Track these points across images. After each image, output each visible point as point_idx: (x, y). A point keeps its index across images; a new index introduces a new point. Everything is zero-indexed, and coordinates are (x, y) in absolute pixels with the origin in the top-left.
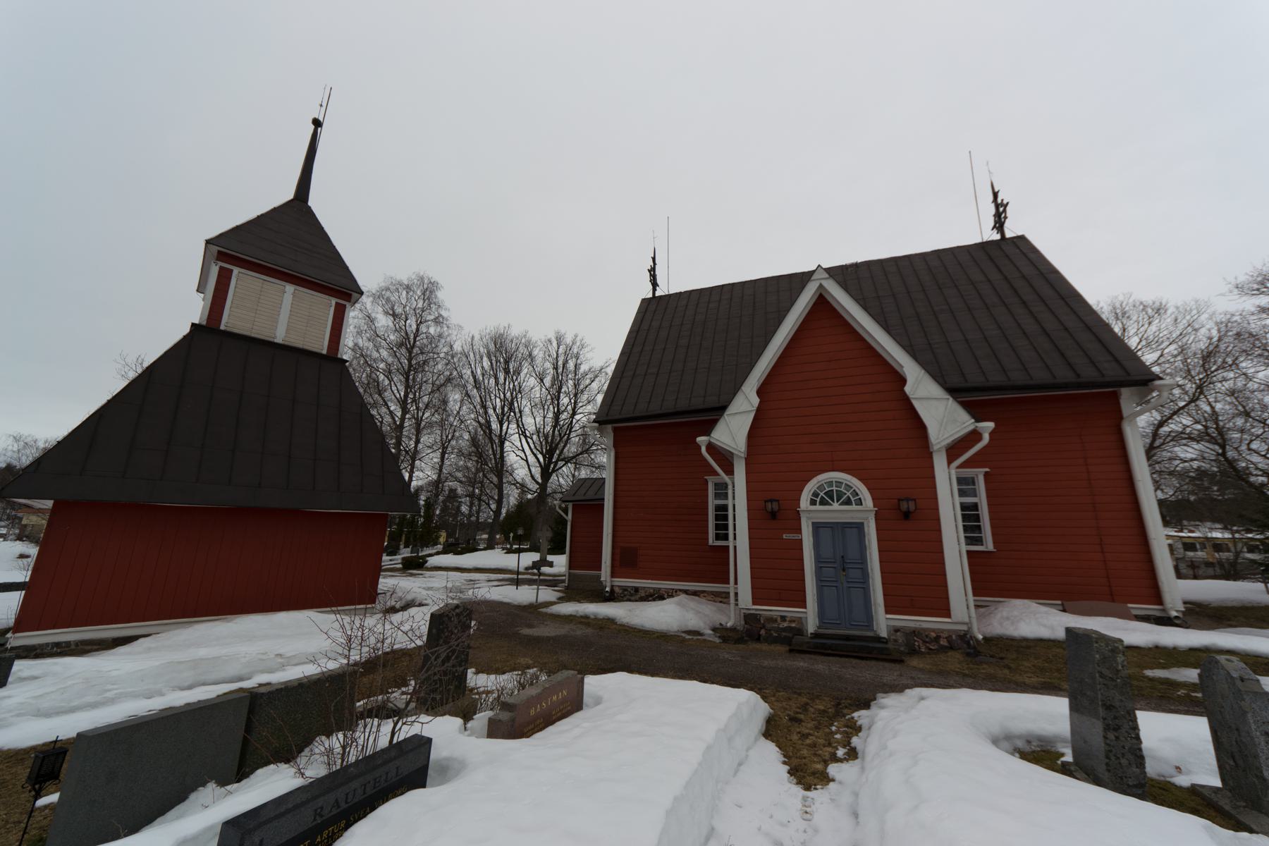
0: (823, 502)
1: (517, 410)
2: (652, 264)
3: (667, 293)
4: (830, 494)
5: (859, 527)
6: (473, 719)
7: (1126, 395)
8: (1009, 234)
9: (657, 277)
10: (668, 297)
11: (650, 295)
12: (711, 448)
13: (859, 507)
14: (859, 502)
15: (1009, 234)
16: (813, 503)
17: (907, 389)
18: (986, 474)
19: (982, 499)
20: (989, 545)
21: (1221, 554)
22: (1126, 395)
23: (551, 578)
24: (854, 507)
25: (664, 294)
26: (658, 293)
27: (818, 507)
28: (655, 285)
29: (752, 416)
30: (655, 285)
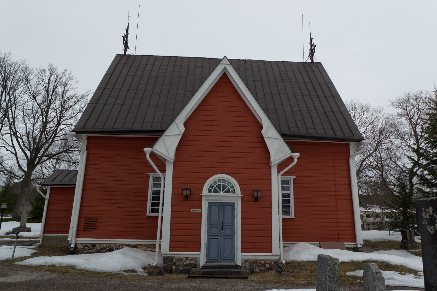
0: (215, 191)
3: (134, 54)
4: (219, 186)
5: (233, 205)
7: (352, 144)
8: (315, 61)
11: (123, 53)
12: (153, 155)
13: (234, 194)
14: (234, 192)
15: (315, 61)
16: (210, 191)
17: (263, 132)
19: (291, 192)
20: (292, 216)
22: (352, 144)
24: (231, 194)
25: (132, 54)
26: (128, 53)
27: (212, 194)
28: (126, 47)
29: (179, 138)
30: (126, 47)
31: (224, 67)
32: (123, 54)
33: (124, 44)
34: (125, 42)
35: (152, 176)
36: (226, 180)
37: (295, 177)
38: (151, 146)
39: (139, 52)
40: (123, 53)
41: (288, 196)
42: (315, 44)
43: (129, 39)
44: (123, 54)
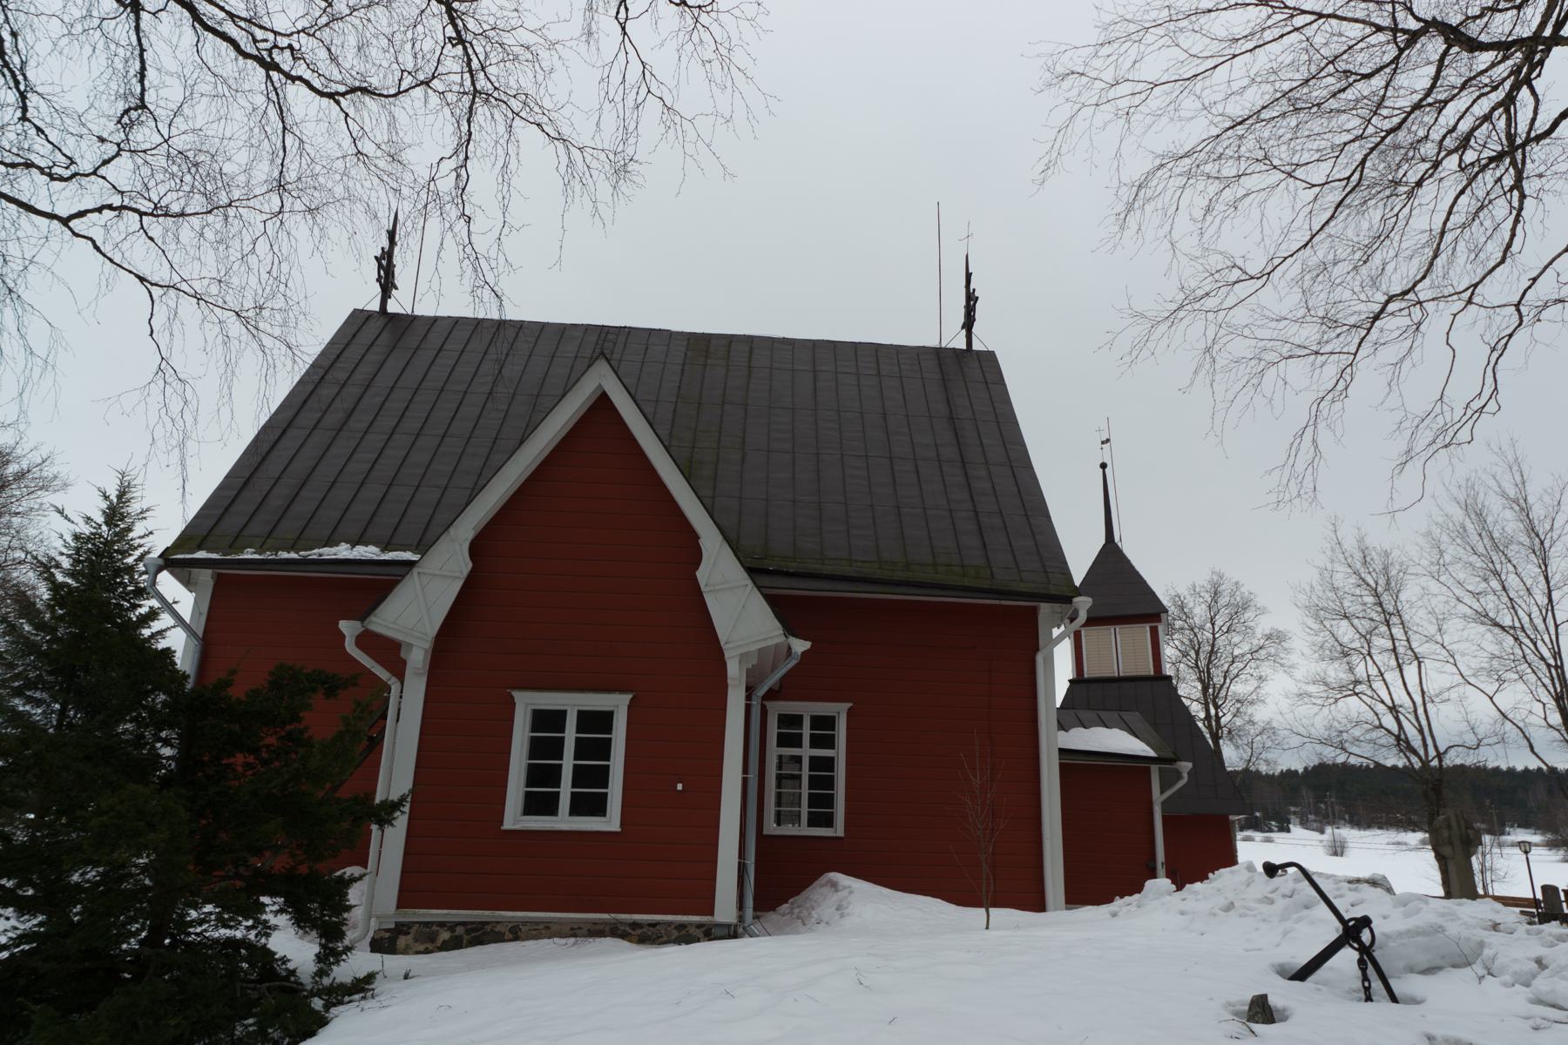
1: (1473, 516)
2: (386, 244)
3: (409, 312)
6: (1207, 878)
7: (1045, 609)
8: (976, 346)
9: (397, 271)
10: (407, 322)
11: (375, 306)
12: (368, 641)
15: (976, 346)
17: (702, 574)
18: (850, 712)
19: (840, 753)
21: (1400, 764)
22: (1045, 609)
23: (1556, 681)
25: (402, 311)
26: (392, 307)
28: (387, 284)
29: (456, 587)
30: (387, 284)
31: (597, 384)
32: (378, 309)
33: (378, 280)
34: (382, 273)
35: (527, 705)
36: (561, 715)
37: (189, 686)
38: (363, 615)
39: (425, 309)
40: (375, 306)
41: (829, 763)
42: (976, 294)
43: (397, 260)
44: (378, 309)
